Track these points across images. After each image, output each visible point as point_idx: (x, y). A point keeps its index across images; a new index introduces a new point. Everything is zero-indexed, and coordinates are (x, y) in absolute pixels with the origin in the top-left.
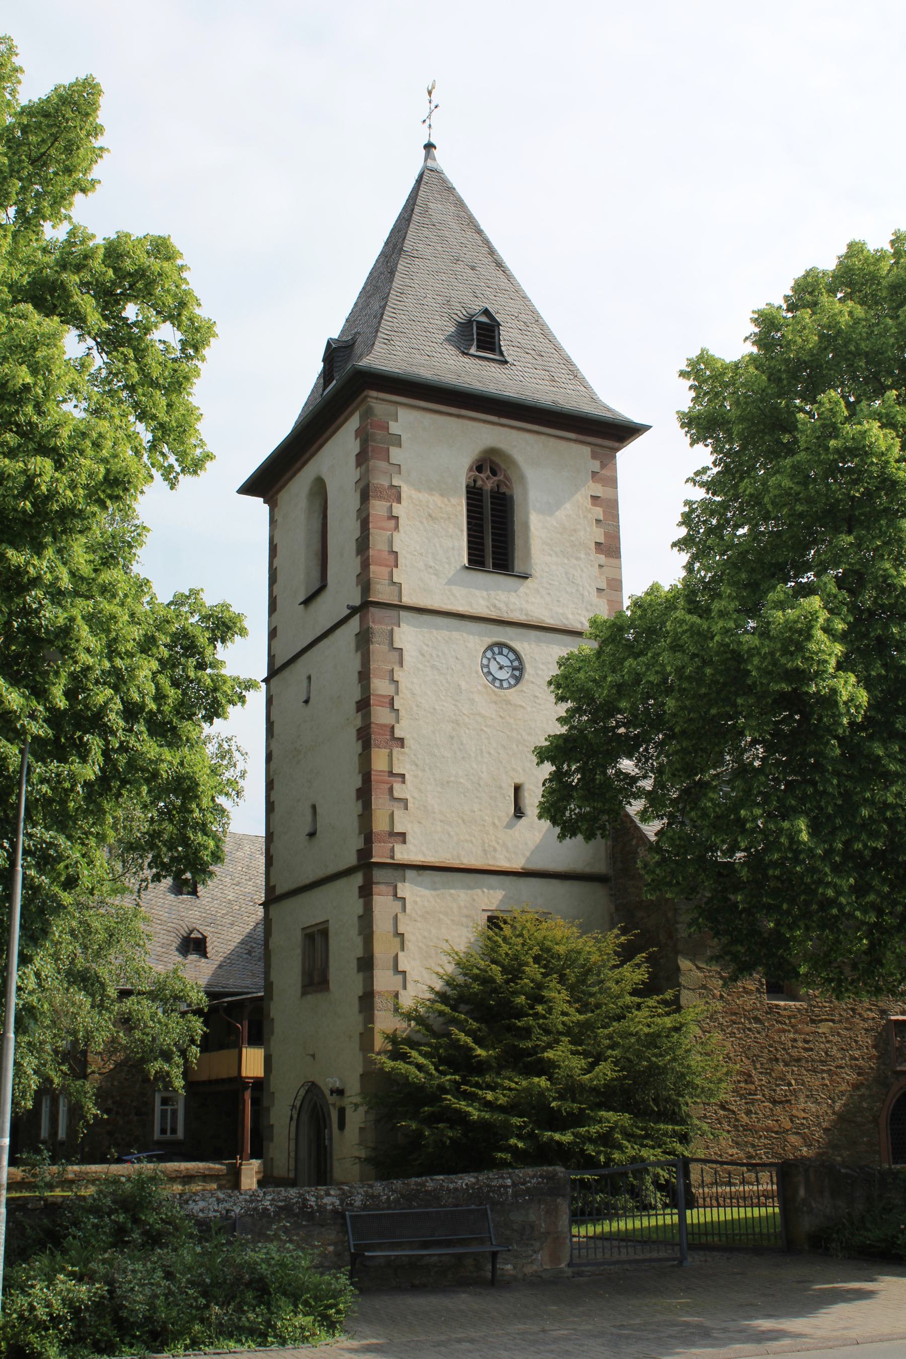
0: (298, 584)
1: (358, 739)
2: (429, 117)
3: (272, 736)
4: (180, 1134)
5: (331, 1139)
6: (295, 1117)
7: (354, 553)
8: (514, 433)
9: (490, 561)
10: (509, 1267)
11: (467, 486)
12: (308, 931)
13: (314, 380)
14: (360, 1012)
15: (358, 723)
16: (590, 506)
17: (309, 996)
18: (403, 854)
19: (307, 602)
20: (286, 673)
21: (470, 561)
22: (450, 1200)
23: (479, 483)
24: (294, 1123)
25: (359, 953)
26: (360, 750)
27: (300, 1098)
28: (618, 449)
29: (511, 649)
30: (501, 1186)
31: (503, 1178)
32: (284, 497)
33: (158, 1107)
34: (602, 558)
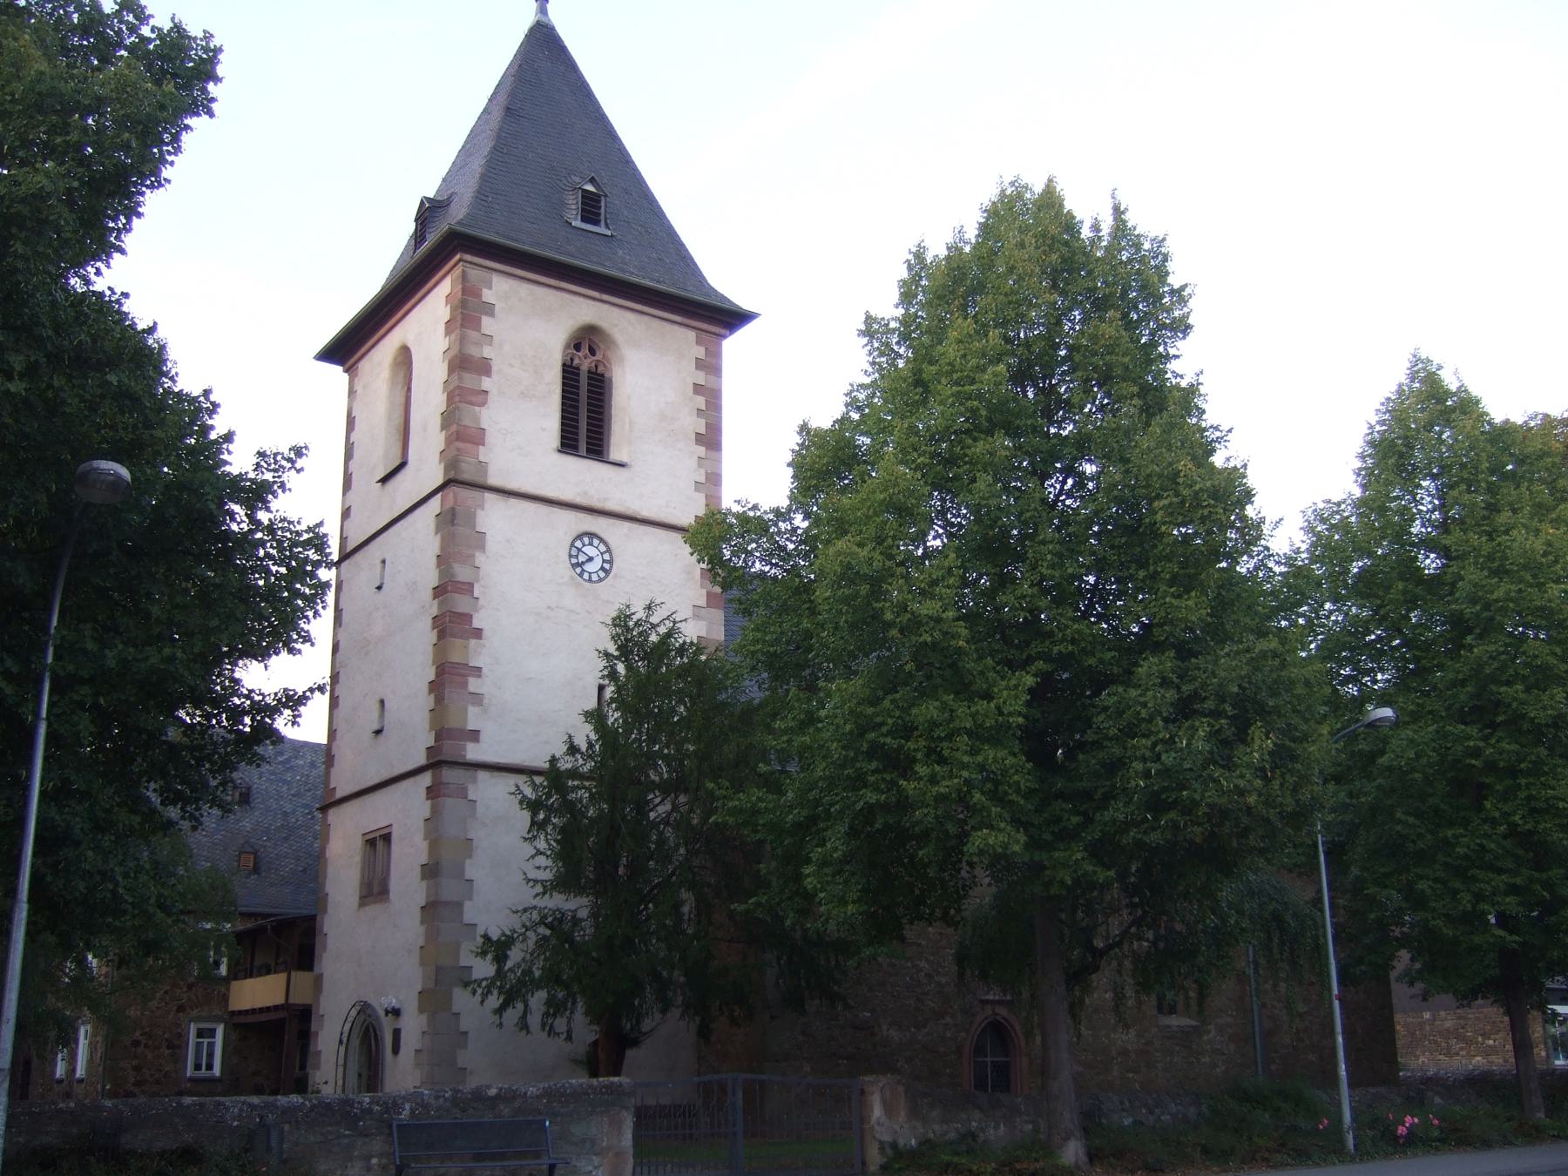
0: (377, 453)
4: (217, 1071)
9: (583, 447)
11: (564, 365)
13: (405, 242)
18: (473, 753)
19: (384, 480)
20: (358, 556)
23: (576, 362)
28: (725, 337)
29: (602, 540)
32: (365, 366)
34: (701, 450)
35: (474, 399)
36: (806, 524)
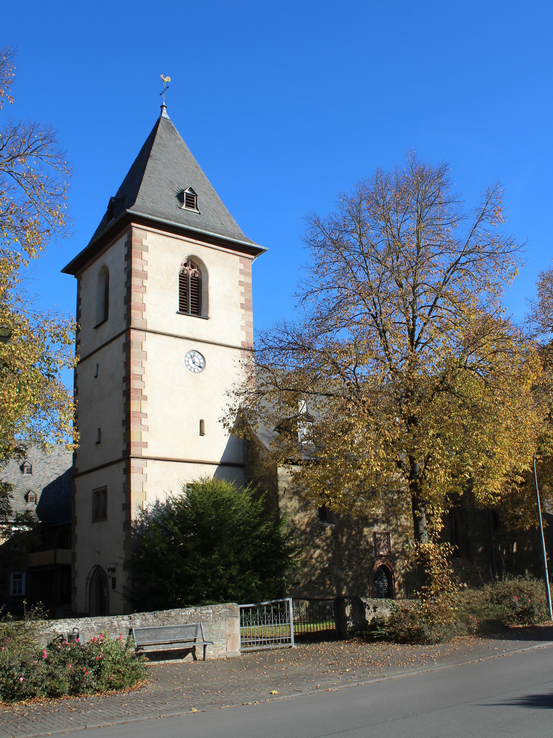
1: (124, 396)
5: (108, 593)
6: (89, 583)
7: (123, 303)
10: (211, 652)
15: (124, 388)
16: (238, 286)
18: (145, 453)
19: (96, 327)
21: (180, 310)
22: (183, 621)
24: (88, 586)
25: (124, 501)
26: (124, 401)
27: (91, 573)
30: (207, 613)
31: (208, 609)
32: (85, 275)
33: (12, 580)
35: (139, 290)
36: (371, 588)
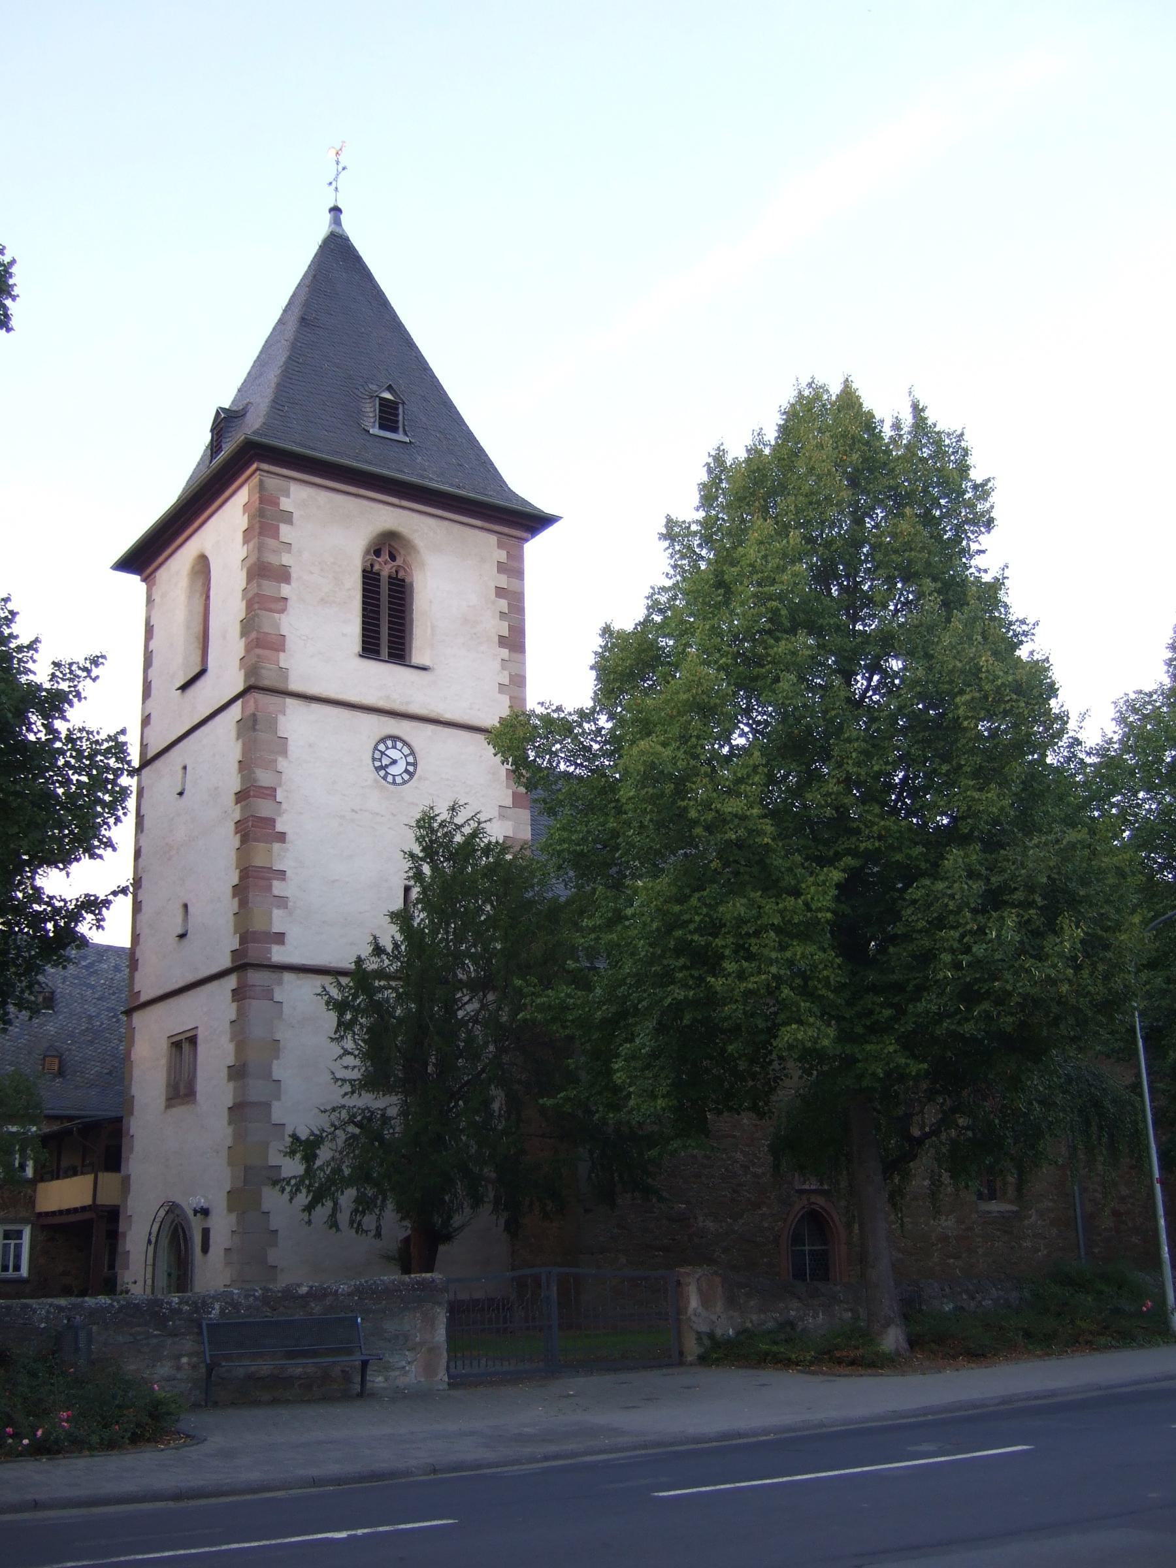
0: (176, 661)
2: (336, 179)
3: (142, 831)
4: (24, 1271)
8: (415, 516)
9: (385, 651)
11: (364, 571)
12: (174, 1040)
14: (230, 1123)
17: (174, 1110)
18: (278, 955)
19: (184, 687)
20: (158, 764)
23: (376, 567)
24: (151, 1248)
28: (527, 540)
29: (405, 743)
32: (163, 575)
34: (505, 653)
35: (273, 606)
